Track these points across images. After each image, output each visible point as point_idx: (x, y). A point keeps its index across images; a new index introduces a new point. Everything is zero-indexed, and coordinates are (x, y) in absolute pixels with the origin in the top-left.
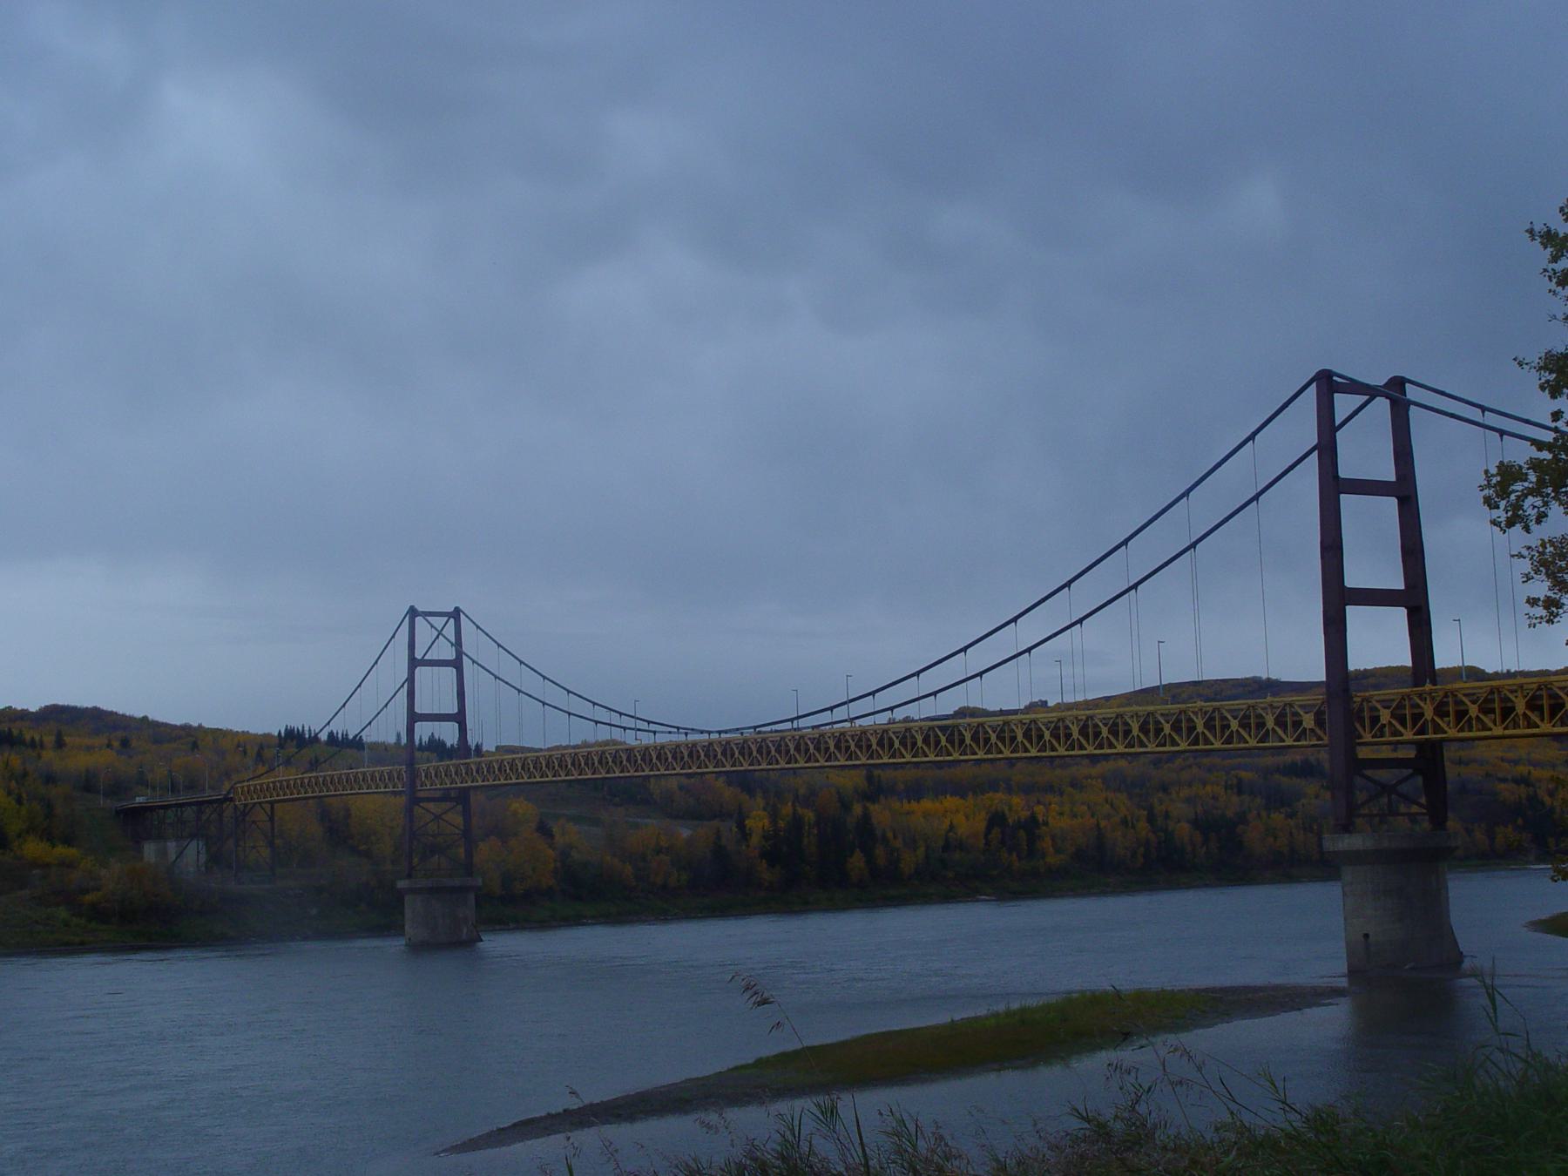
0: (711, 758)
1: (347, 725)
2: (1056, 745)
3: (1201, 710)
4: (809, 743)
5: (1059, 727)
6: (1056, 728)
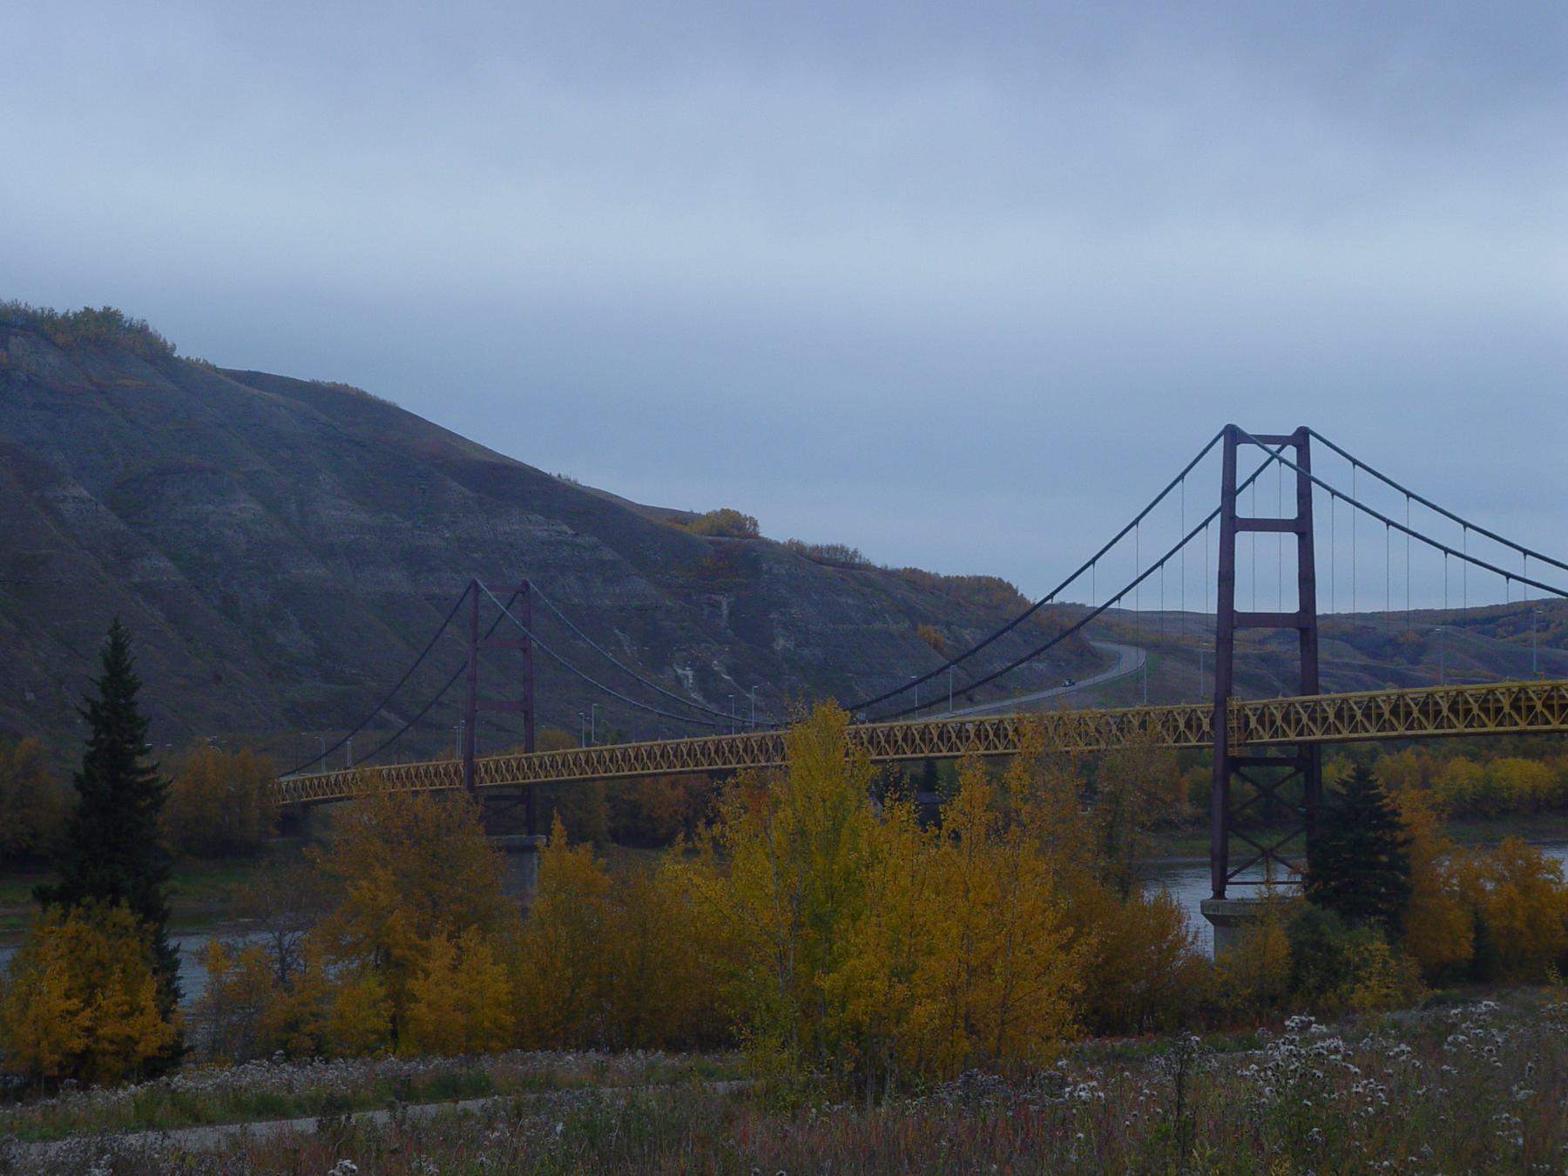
0: (964, 739)
1: (1087, 594)
2: (1550, 717)
3: (1184, 711)
4: (1355, 707)
5: (1458, 702)
6: (1368, 707)
